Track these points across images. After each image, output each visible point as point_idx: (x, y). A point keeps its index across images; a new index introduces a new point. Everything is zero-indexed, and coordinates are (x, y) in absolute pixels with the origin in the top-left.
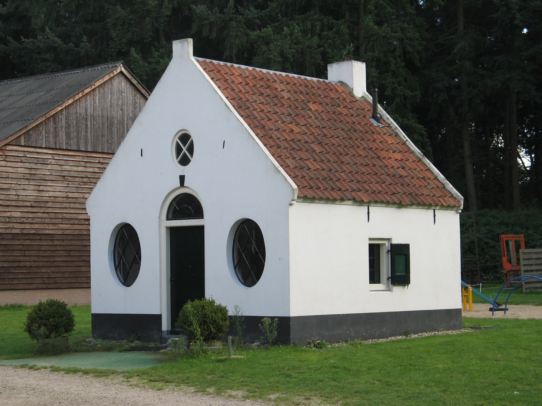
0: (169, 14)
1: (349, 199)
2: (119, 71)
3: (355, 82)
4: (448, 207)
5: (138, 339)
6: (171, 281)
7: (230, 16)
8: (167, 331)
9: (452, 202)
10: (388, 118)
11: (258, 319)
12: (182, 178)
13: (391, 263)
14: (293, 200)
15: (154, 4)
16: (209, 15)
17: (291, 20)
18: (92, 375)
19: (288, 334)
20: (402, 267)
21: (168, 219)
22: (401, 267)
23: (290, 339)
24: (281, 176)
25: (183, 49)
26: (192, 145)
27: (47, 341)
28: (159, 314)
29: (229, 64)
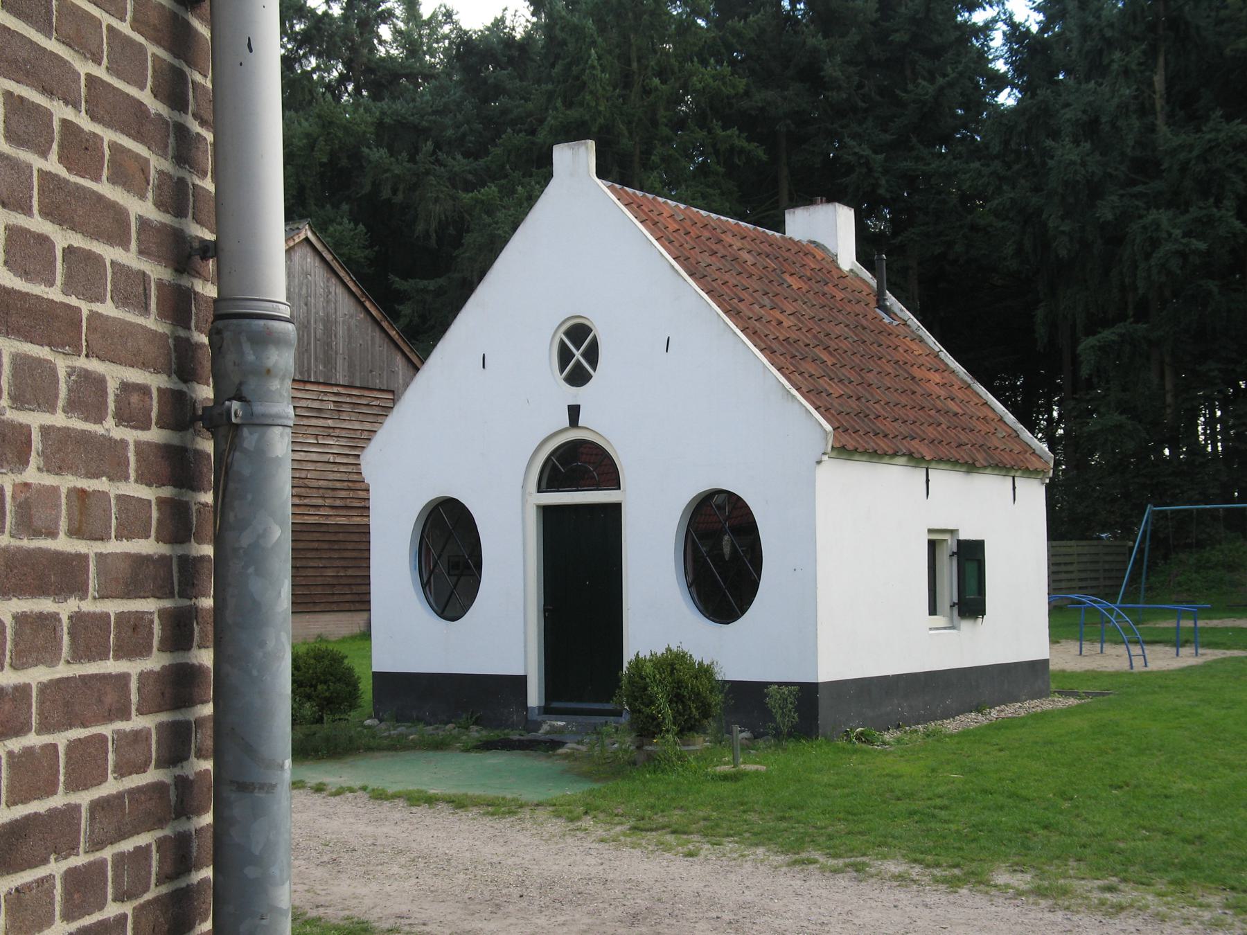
1: (904, 455)
2: (302, 236)
3: (840, 243)
4: (1030, 473)
5: (476, 723)
8: (539, 707)
11: (758, 689)
12: (574, 411)
13: (961, 576)
14: (824, 454)
15: (300, 144)
18: (475, 810)
19: (815, 717)
21: (539, 491)
22: (972, 583)
23: (817, 727)
24: (796, 406)
25: (574, 162)
26: (594, 346)
27: (315, 727)
28: (522, 673)
29: (650, 196)
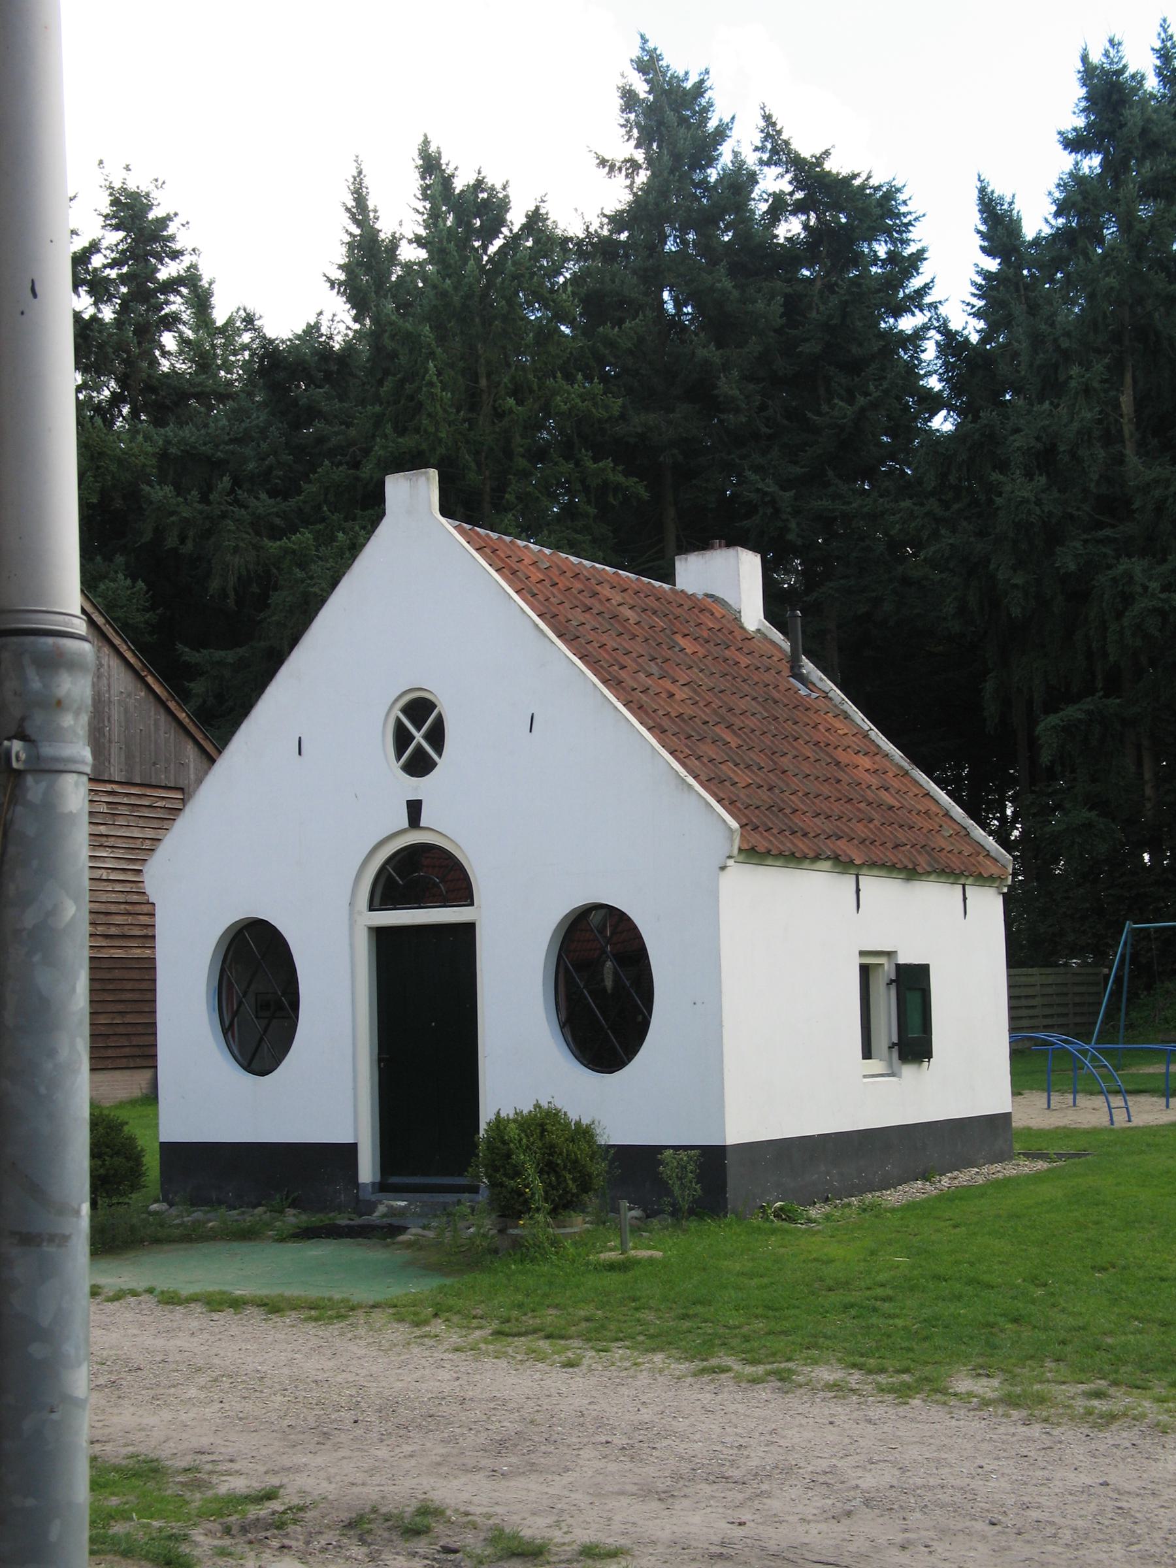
0: (95, 501)
1: (828, 858)
3: (744, 597)
5: (293, 1205)
6: (380, 1060)
7: (223, 507)
8: (373, 1184)
9: (994, 870)
10: (821, 679)
11: (649, 1154)
12: (414, 809)
14: (730, 857)
16: (178, 505)
17: (346, 519)
18: (294, 1314)
20: (915, 1019)
21: (371, 908)
22: (915, 1019)
23: (725, 1200)
25: (412, 497)
29: (507, 539)
